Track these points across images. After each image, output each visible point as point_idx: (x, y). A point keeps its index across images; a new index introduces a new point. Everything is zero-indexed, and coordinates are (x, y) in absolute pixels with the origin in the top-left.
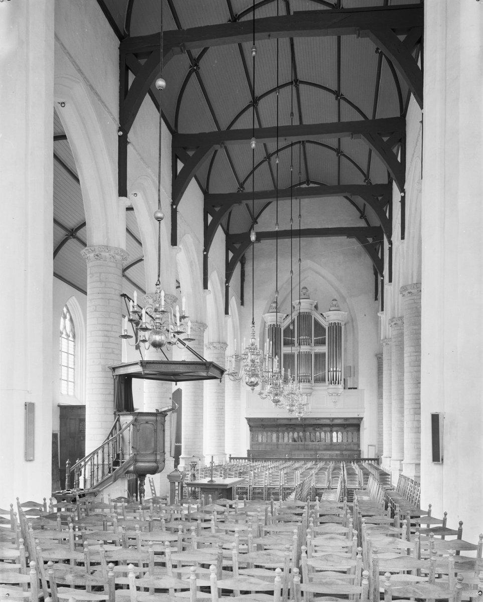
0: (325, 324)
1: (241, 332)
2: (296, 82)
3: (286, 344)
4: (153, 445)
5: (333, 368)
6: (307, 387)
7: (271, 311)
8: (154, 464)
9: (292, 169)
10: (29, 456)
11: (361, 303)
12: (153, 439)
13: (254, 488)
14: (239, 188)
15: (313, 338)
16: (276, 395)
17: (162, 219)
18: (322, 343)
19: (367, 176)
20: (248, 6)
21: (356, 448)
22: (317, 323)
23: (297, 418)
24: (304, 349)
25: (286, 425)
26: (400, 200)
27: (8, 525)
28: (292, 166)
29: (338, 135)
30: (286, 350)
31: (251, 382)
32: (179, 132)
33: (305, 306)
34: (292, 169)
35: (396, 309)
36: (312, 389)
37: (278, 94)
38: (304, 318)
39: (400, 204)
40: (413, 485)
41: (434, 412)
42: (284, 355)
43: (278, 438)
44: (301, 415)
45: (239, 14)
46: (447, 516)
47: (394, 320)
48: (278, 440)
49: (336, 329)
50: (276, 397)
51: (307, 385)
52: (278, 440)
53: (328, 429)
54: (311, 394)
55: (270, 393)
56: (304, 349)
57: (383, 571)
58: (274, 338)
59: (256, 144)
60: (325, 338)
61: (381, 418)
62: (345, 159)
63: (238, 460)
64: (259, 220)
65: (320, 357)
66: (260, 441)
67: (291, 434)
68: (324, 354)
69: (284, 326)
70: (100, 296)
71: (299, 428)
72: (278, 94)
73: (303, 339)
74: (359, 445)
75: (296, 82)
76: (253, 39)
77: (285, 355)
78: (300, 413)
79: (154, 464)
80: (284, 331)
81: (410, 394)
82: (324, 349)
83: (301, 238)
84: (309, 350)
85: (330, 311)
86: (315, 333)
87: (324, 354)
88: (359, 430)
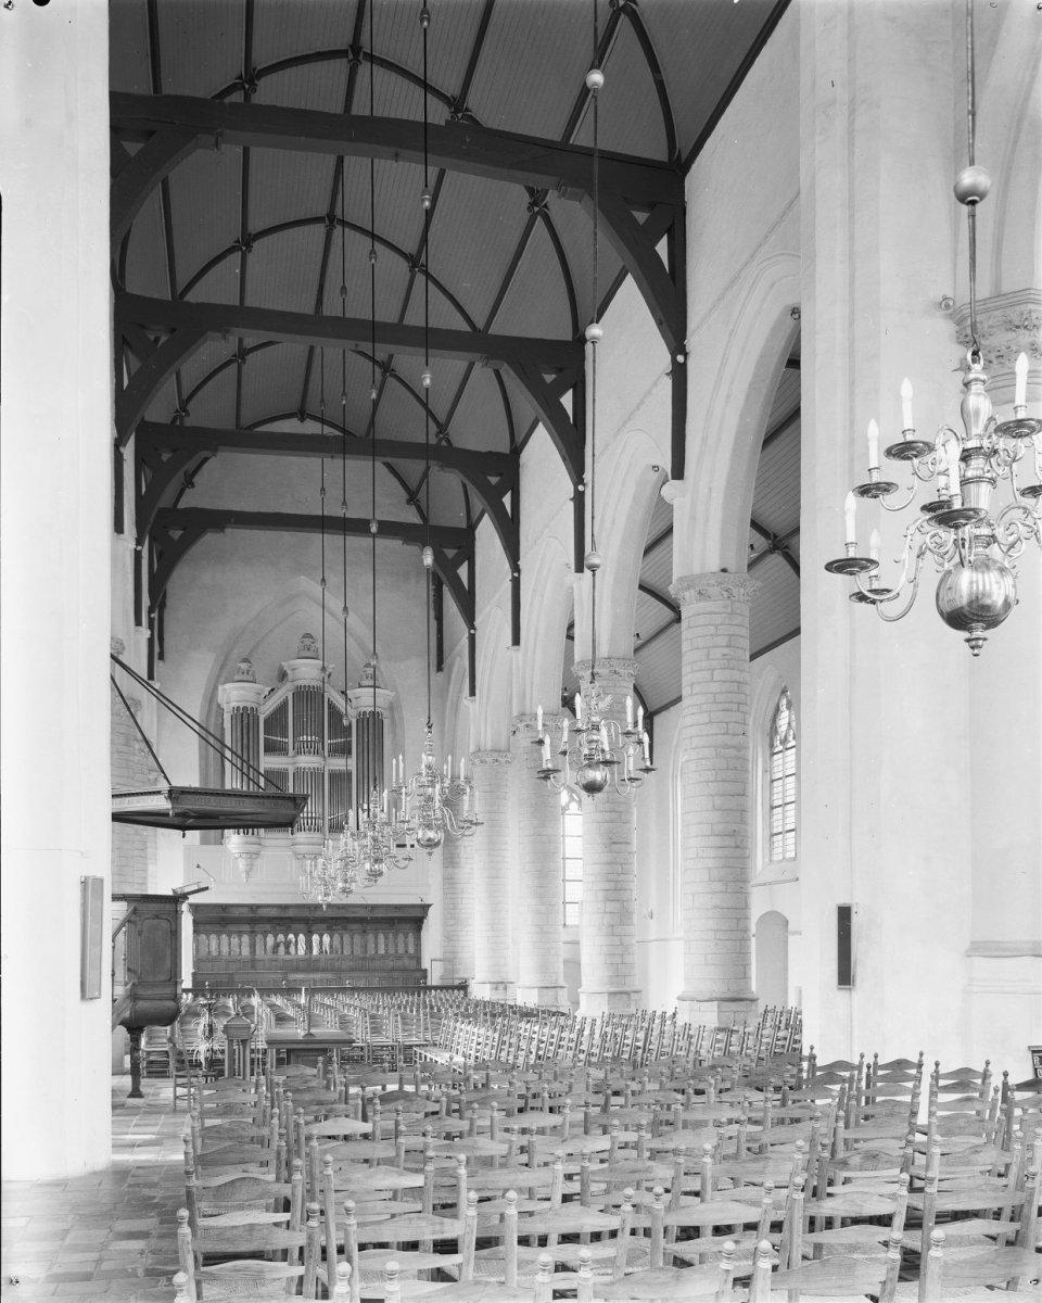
1: (158, 717)
2: (331, 220)
3: (271, 748)
4: (168, 963)
6: (315, 840)
7: (236, 678)
8: (171, 1004)
9: (344, 402)
10: (85, 993)
11: (407, 675)
12: (169, 952)
13: (149, 1053)
14: (177, 411)
16: (377, 861)
17: (598, 566)
18: (345, 751)
19: (442, 428)
21: (413, 964)
23: (318, 907)
25: (270, 920)
26: (572, 496)
27: (211, 1124)
28: (344, 394)
29: (470, 356)
31: (429, 840)
32: (127, 290)
33: (307, 672)
34: (344, 402)
35: (528, 697)
36: (260, 844)
37: (373, 261)
38: (308, 697)
39: (571, 504)
40: (496, 1035)
41: (843, 901)
42: (330, 775)
43: (253, 946)
44: (330, 899)
45: (259, 68)
46: (990, 1067)
47: (525, 718)
48: (253, 951)
49: (372, 724)
50: (376, 866)
51: (317, 835)
52: (253, 951)
53: (246, 928)
54: (258, 854)
56: (307, 761)
58: (245, 736)
59: (431, 379)
62: (398, 384)
63: (456, 991)
64: (196, 479)
65: (339, 779)
66: (215, 953)
67: (270, 940)
69: (266, 710)
71: (298, 926)
72: (373, 261)
73: (307, 741)
74: (418, 959)
75: (331, 220)
78: (326, 895)
79: (171, 1004)
81: (596, 864)
83: (347, 537)
85: (360, 686)
86: (329, 732)
88: (419, 929)
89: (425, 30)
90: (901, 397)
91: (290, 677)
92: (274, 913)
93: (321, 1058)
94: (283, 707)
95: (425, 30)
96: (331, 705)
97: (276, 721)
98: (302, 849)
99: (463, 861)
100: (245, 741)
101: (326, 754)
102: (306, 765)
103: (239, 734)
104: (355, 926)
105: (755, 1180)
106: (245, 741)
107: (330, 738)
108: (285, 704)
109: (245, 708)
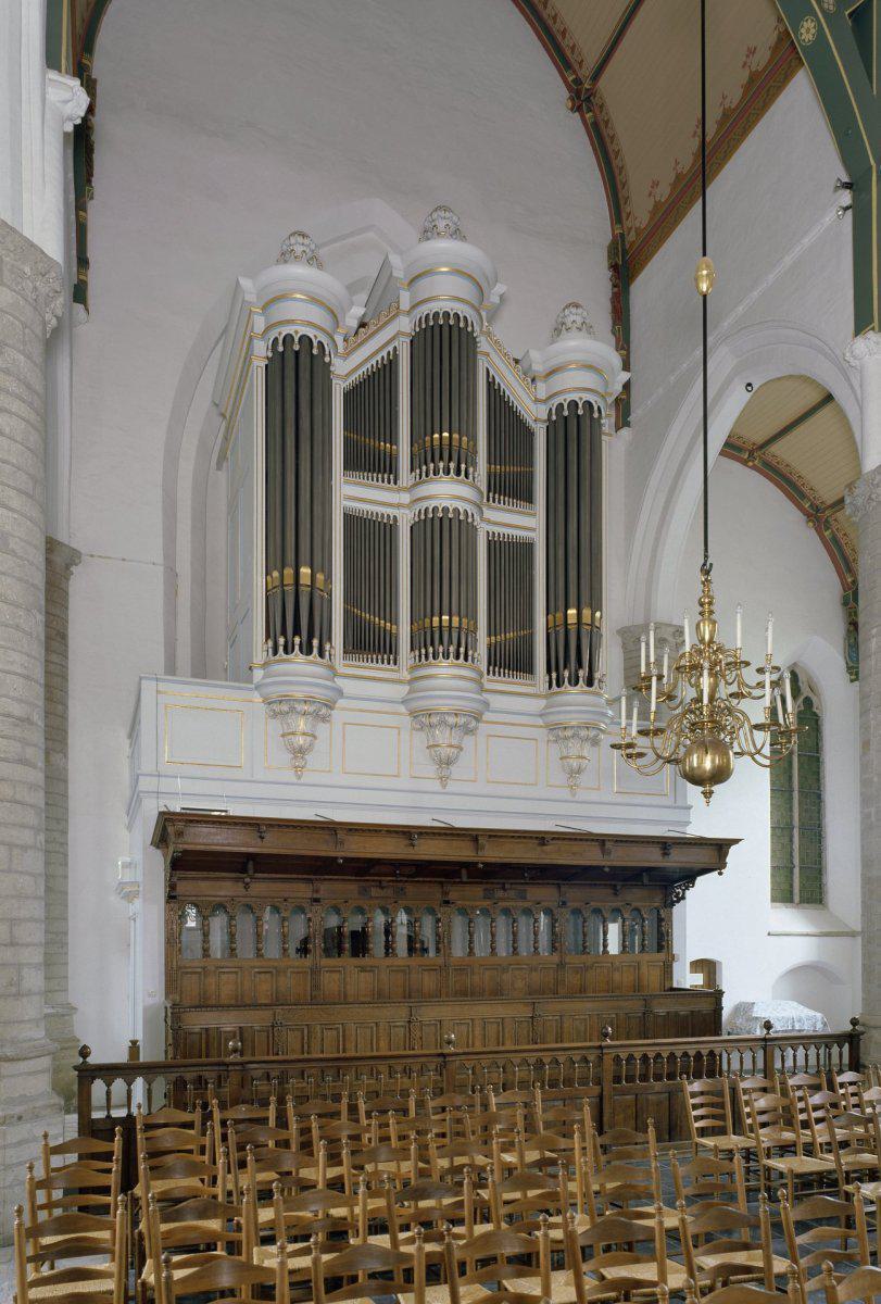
0: (533, 411)
3: (371, 461)
24: (448, 492)
30: (351, 494)
69: (346, 370)
77: (351, 520)
97: (372, 394)
102: (451, 504)
108: (388, 368)
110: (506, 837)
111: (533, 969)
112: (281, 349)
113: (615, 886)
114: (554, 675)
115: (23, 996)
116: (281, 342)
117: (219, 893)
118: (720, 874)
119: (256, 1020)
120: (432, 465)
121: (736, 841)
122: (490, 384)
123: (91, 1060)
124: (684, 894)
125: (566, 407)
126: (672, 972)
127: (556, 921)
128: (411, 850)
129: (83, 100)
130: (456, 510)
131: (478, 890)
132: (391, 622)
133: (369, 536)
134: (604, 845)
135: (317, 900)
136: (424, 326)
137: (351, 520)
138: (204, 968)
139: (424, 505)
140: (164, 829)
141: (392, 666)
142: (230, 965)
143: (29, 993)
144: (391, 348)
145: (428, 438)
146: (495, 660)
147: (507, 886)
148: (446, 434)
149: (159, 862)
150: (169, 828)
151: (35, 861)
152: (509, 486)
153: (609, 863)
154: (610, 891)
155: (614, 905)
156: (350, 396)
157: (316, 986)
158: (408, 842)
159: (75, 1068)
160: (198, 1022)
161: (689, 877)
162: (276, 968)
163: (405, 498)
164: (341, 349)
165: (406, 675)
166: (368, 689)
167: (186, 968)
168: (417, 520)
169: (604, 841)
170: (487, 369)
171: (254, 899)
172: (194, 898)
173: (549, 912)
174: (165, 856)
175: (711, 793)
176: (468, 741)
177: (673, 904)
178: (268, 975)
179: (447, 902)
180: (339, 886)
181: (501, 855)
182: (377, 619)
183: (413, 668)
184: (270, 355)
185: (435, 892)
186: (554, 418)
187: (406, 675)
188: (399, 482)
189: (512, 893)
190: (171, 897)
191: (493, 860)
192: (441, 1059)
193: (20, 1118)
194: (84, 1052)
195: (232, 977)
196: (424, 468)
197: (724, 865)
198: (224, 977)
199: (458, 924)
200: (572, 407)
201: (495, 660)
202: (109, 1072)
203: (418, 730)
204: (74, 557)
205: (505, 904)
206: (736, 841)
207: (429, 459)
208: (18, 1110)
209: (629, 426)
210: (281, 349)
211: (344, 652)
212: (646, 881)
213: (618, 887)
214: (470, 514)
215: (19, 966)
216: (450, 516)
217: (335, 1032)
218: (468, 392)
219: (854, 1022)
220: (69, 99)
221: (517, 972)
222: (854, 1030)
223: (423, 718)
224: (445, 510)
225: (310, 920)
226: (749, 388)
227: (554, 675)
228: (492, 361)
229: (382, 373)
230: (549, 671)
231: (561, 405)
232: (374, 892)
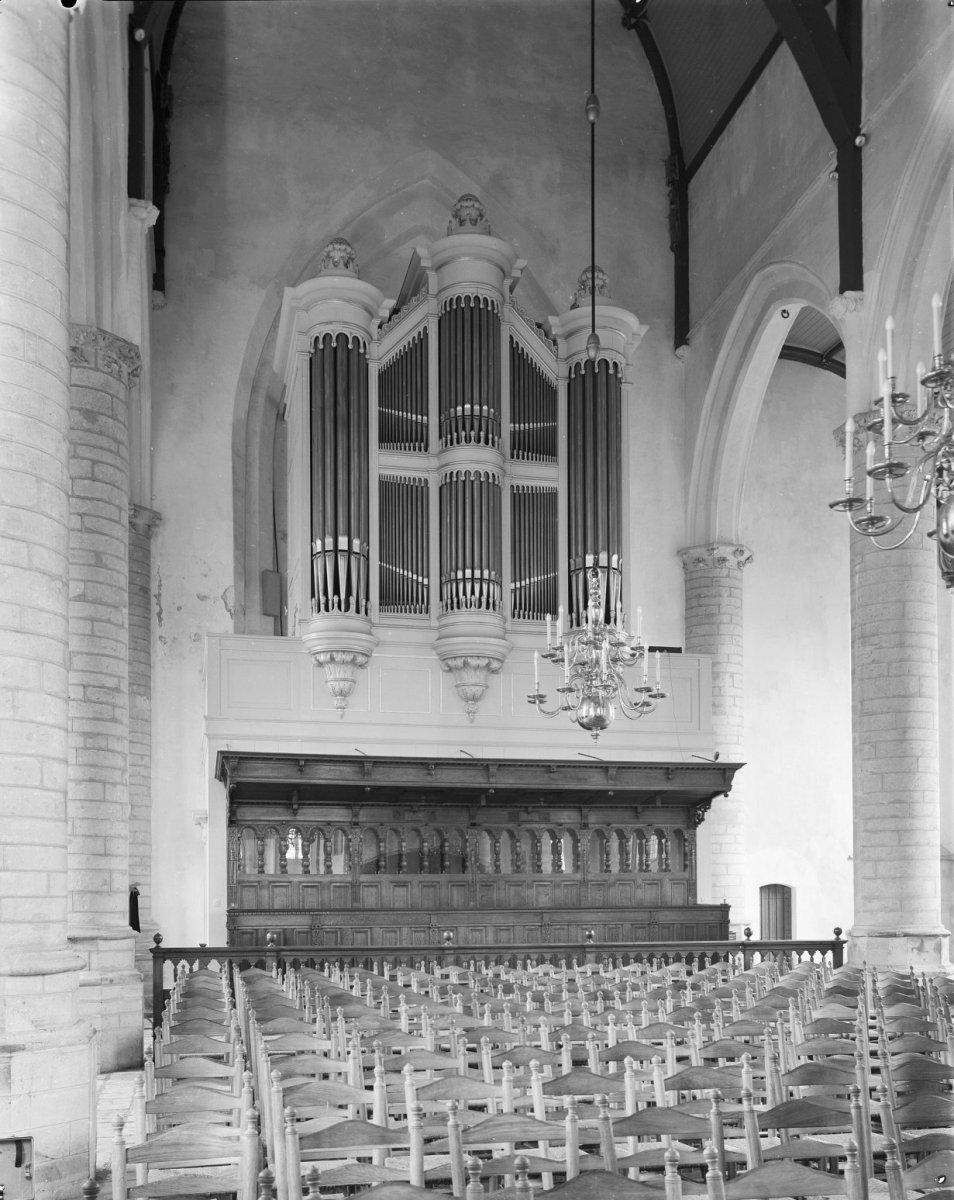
0: (552, 367)
3: (395, 435)
5: (596, 553)
15: (507, 427)
20: (800, 343)
22: (520, 361)
24: (471, 458)
28: (593, 98)
30: (387, 463)
38: (468, 324)
55: (136, 369)
57: (355, 1183)
58: (341, 399)
60: (554, 430)
61: (694, 603)
65: (533, 505)
68: (552, 496)
69: (381, 353)
70: (77, 609)
76: (596, 7)
77: (385, 486)
80: (381, 377)
82: (549, 475)
84: (491, 469)
87: (552, 496)
88: (694, 821)
89: (593, 124)
90: (709, 804)
91: (433, 287)
92: (346, 776)
93: (783, 442)
94: (416, 351)
95: (593, 124)
96: (519, 358)
97: (404, 374)
98: (460, 645)
99: (728, 701)
100: (342, 409)
101: (508, 613)
102: (473, 468)
103: (328, 391)
104: (568, 817)
105: (175, 1122)
106: (342, 409)
107: (513, 421)
108: (422, 342)
109: (342, 337)
110: (514, 766)
111: (557, 886)
112: (321, 346)
113: (636, 808)
114: (574, 615)
115: (115, 892)
116: (321, 340)
117: (262, 818)
118: (726, 796)
119: (299, 922)
120: (463, 434)
121: (740, 766)
122: (515, 350)
123: (163, 945)
124: (703, 815)
125: (583, 365)
126: (696, 889)
127: (579, 841)
128: (429, 778)
129: (156, 213)
130: (478, 473)
131: (504, 813)
132: (417, 574)
133: (402, 498)
134: (724, 773)
135: (356, 824)
136: (448, 309)
137: (385, 486)
138: (259, 882)
139: (448, 470)
140: (223, 766)
141: (424, 615)
142: (282, 880)
143: (118, 891)
144: (421, 329)
145: (452, 410)
146: (520, 604)
147: (530, 809)
148: (468, 406)
149: (222, 793)
150: (230, 764)
151: (204, 1091)
152: (534, 446)
153: (369, 783)
154: (632, 814)
155: (637, 826)
156: (383, 377)
157: (356, 899)
158: (426, 772)
159: (151, 950)
160: (249, 922)
161: (705, 802)
162: (320, 882)
163: (434, 463)
164: (375, 337)
165: (434, 623)
166: (402, 641)
167: (244, 882)
168: (444, 483)
169: (607, 768)
170: (511, 337)
171: (301, 823)
172: (250, 823)
173: (572, 833)
174: (226, 785)
175: (597, 735)
176: (494, 679)
177: (696, 825)
178: (315, 889)
179: (473, 825)
180: (377, 811)
181: (511, 781)
182: (410, 573)
183: (439, 617)
184: (313, 351)
185: (462, 818)
186: (573, 376)
187: (434, 623)
188: (430, 449)
189: (535, 817)
190: (232, 822)
191: (503, 786)
192: (439, 952)
193: (111, 981)
194: (158, 939)
195: (284, 890)
196: (449, 436)
197: (729, 788)
198: (277, 890)
199: (486, 842)
200: (589, 367)
201: (520, 604)
202: (177, 954)
203: (448, 671)
204: (156, 519)
205: (528, 826)
206: (740, 766)
207: (454, 431)
208: (110, 976)
209: (687, 344)
210: (321, 346)
211: (380, 604)
212: (659, 804)
213: (640, 810)
214: (491, 475)
215: (110, 871)
216: (472, 478)
217: (363, 935)
218: (359, 506)
219: (838, 932)
220: (150, 214)
221: (541, 889)
222: (838, 938)
223: (453, 664)
224: (467, 473)
225: (350, 840)
226: (785, 315)
227: (574, 615)
228: (516, 328)
229: (414, 352)
230: (571, 611)
231: (578, 365)
232: (408, 816)
